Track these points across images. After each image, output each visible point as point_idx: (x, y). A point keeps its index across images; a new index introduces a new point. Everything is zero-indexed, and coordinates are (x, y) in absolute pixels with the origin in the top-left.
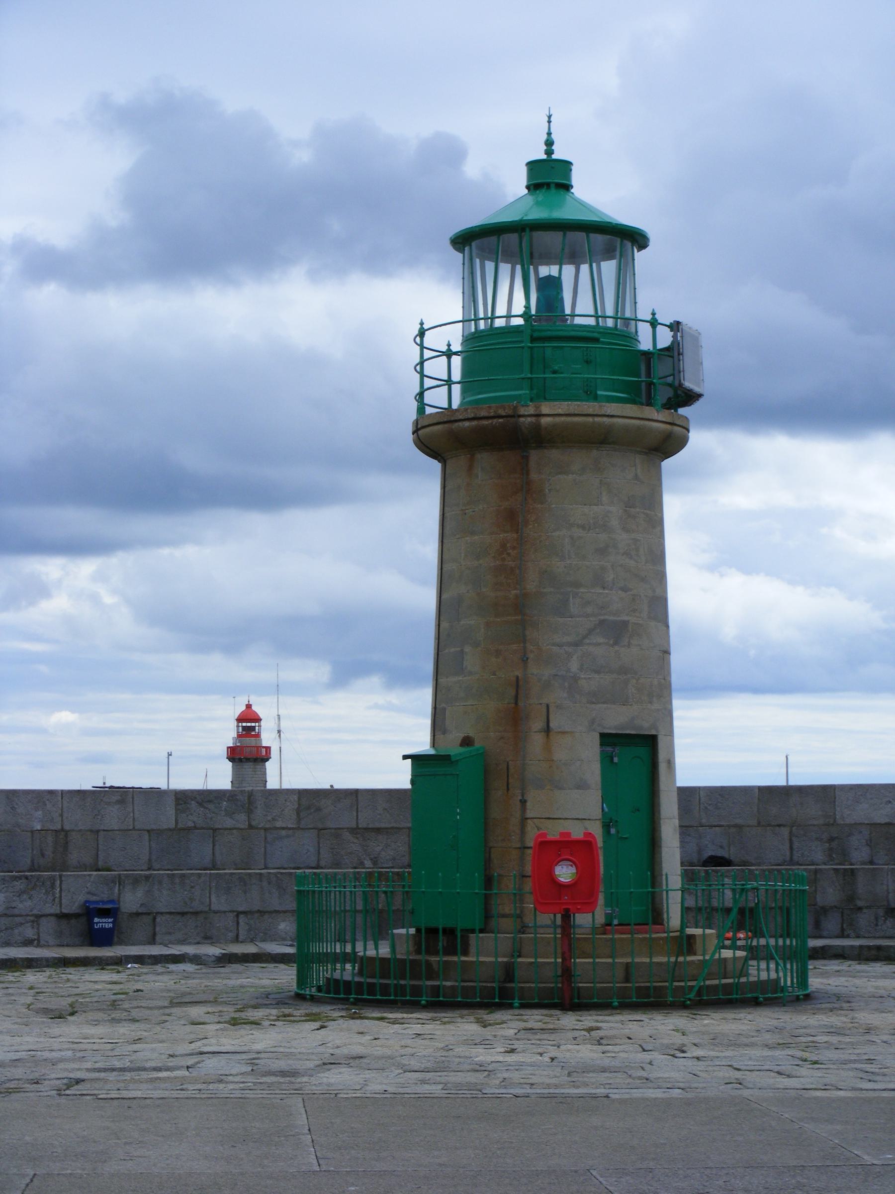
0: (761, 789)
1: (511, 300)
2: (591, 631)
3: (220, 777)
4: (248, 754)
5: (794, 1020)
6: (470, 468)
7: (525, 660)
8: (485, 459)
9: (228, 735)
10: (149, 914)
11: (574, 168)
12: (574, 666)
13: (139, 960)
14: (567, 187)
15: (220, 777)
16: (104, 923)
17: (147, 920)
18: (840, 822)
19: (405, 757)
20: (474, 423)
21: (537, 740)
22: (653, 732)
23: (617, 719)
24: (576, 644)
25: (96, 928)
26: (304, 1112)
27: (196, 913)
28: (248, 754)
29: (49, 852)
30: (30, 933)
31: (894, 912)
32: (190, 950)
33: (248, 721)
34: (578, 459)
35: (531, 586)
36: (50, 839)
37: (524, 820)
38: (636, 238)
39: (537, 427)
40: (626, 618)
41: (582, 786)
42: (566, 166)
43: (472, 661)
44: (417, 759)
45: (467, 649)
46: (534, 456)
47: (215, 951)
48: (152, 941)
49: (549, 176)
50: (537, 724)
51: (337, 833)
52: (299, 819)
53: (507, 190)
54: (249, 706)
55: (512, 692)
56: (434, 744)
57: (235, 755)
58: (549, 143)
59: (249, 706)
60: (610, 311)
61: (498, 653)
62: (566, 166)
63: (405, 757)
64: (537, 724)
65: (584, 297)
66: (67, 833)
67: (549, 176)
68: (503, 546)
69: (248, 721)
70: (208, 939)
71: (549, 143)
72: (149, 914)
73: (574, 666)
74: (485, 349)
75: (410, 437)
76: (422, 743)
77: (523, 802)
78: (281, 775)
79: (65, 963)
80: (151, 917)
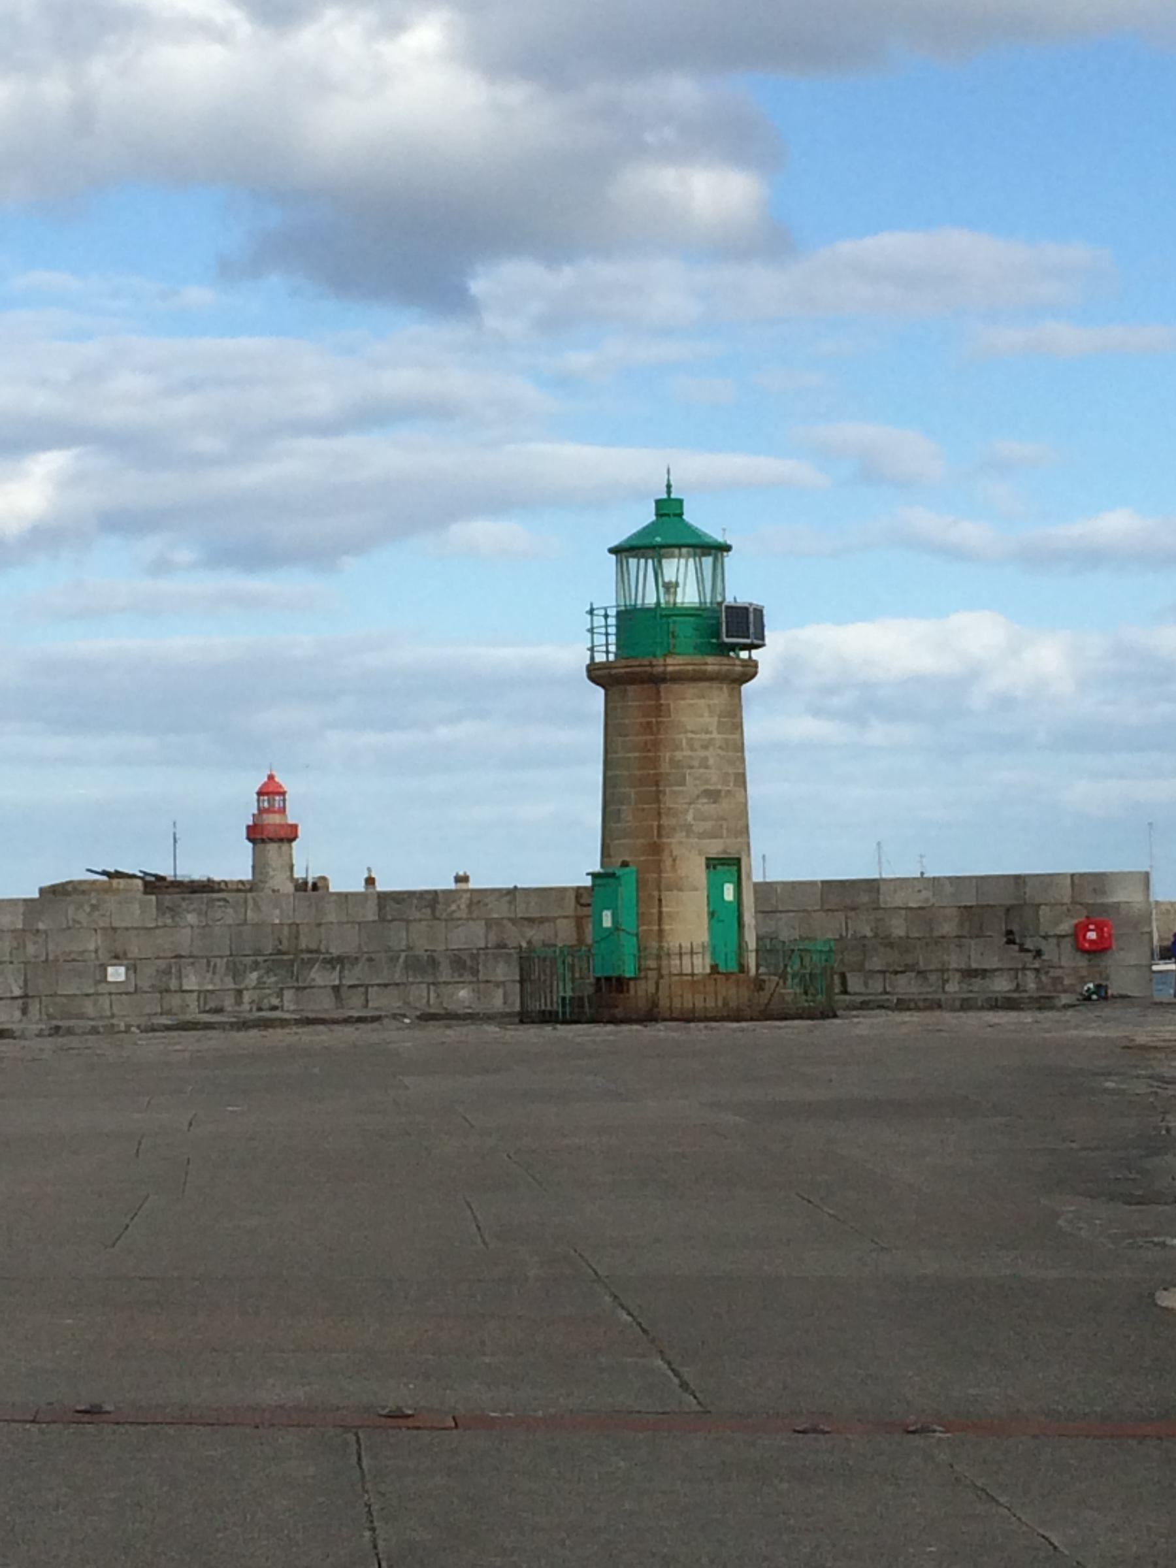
2: (698, 797)
10: (361, 986)
12: (690, 818)
14: (681, 515)
17: (362, 989)
18: (883, 906)
19: (588, 874)
20: (628, 670)
22: (737, 856)
23: (715, 848)
24: (690, 804)
27: (397, 984)
28: (269, 834)
29: (285, 942)
31: (1174, 1051)
33: (270, 791)
36: (286, 930)
40: (719, 787)
42: (680, 502)
44: (595, 876)
46: (663, 686)
51: (498, 922)
52: (470, 912)
54: (271, 777)
56: (602, 865)
57: (256, 834)
58: (669, 486)
59: (271, 777)
60: (708, 600)
62: (680, 502)
63: (588, 874)
66: (298, 925)
69: (270, 791)
71: (669, 486)
72: (361, 986)
73: (690, 818)
75: (585, 674)
76: (597, 868)
80: (826, 907)
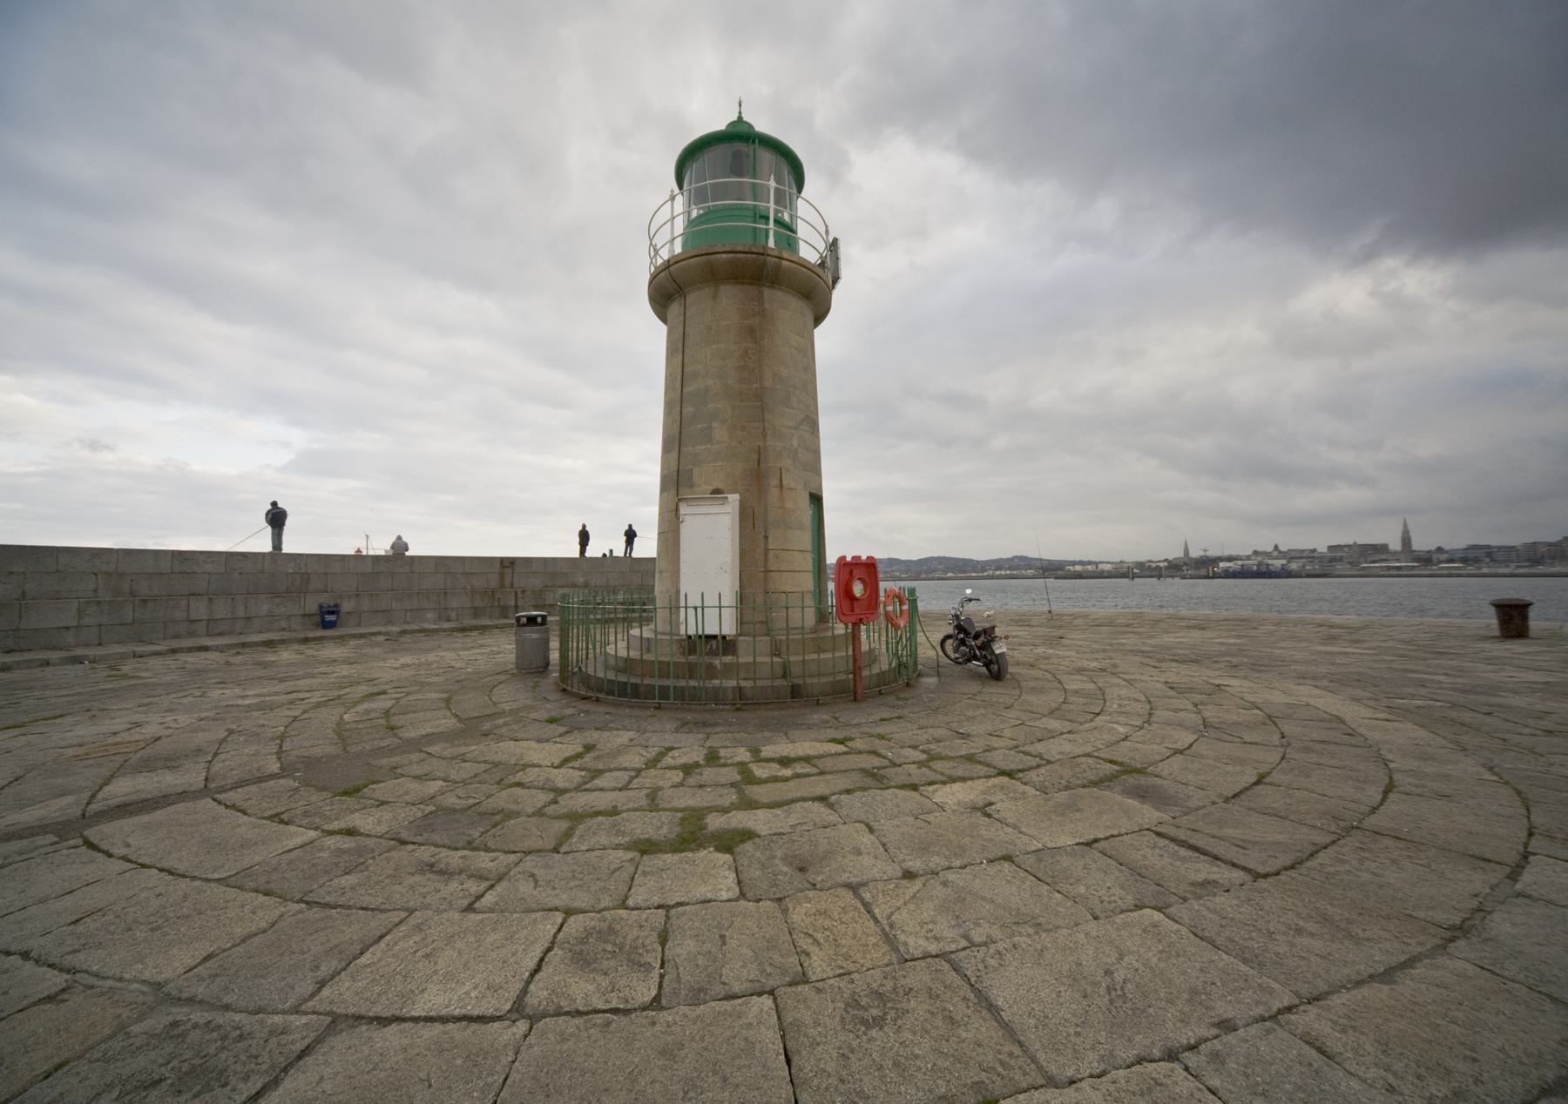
0: (502, 560)
6: (715, 296)
7: (764, 435)
11: (288, 522)
12: (795, 443)
13: (354, 636)
16: (332, 618)
21: (774, 493)
26: (1041, 1056)
28: (1186, 551)
30: (284, 624)
32: (383, 629)
35: (768, 383)
37: (767, 550)
39: (778, 267)
41: (801, 528)
43: (720, 433)
45: (715, 425)
47: (395, 629)
48: (359, 625)
50: (774, 482)
55: (756, 457)
61: (743, 428)
64: (774, 482)
68: (746, 351)
70: (390, 622)
77: (766, 537)
79: (306, 640)
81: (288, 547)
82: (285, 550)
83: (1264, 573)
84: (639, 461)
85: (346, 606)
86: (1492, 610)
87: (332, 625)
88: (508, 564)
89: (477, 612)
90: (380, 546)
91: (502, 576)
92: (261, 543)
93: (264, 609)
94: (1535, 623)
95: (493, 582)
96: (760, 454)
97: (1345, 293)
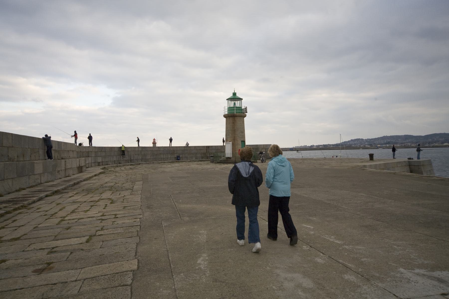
0: (207, 146)
1: (232, 104)
3: (151, 145)
4: (154, 143)
5: (301, 156)
8: (231, 118)
9: (152, 141)
15: (151, 145)
23: (242, 140)
25: (178, 159)
28: (154, 143)
34: (239, 118)
38: (242, 99)
43: (230, 135)
49: (234, 94)
53: (230, 95)
65: (238, 104)
67: (234, 94)
74: (230, 109)
78: (158, 145)
81: (141, 145)
82: (93, 145)
83: (321, 149)
84: (223, 134)
85: (181, 156)
86: (368, 156)
87: (179, 159)
88: (208, 147)
89: (202, 158)
90: (184, 145)
91: (207, 150)
92: (168, 145)
93: (170, 156)
94: (374, 158)
95: (205, 151)
96: (234, 137)
97: (321, 96)
